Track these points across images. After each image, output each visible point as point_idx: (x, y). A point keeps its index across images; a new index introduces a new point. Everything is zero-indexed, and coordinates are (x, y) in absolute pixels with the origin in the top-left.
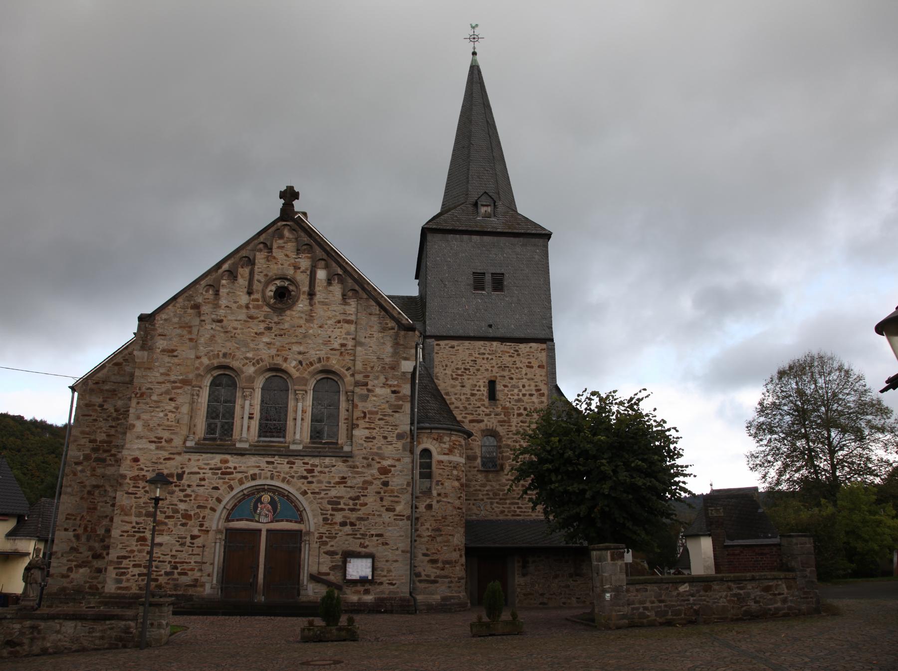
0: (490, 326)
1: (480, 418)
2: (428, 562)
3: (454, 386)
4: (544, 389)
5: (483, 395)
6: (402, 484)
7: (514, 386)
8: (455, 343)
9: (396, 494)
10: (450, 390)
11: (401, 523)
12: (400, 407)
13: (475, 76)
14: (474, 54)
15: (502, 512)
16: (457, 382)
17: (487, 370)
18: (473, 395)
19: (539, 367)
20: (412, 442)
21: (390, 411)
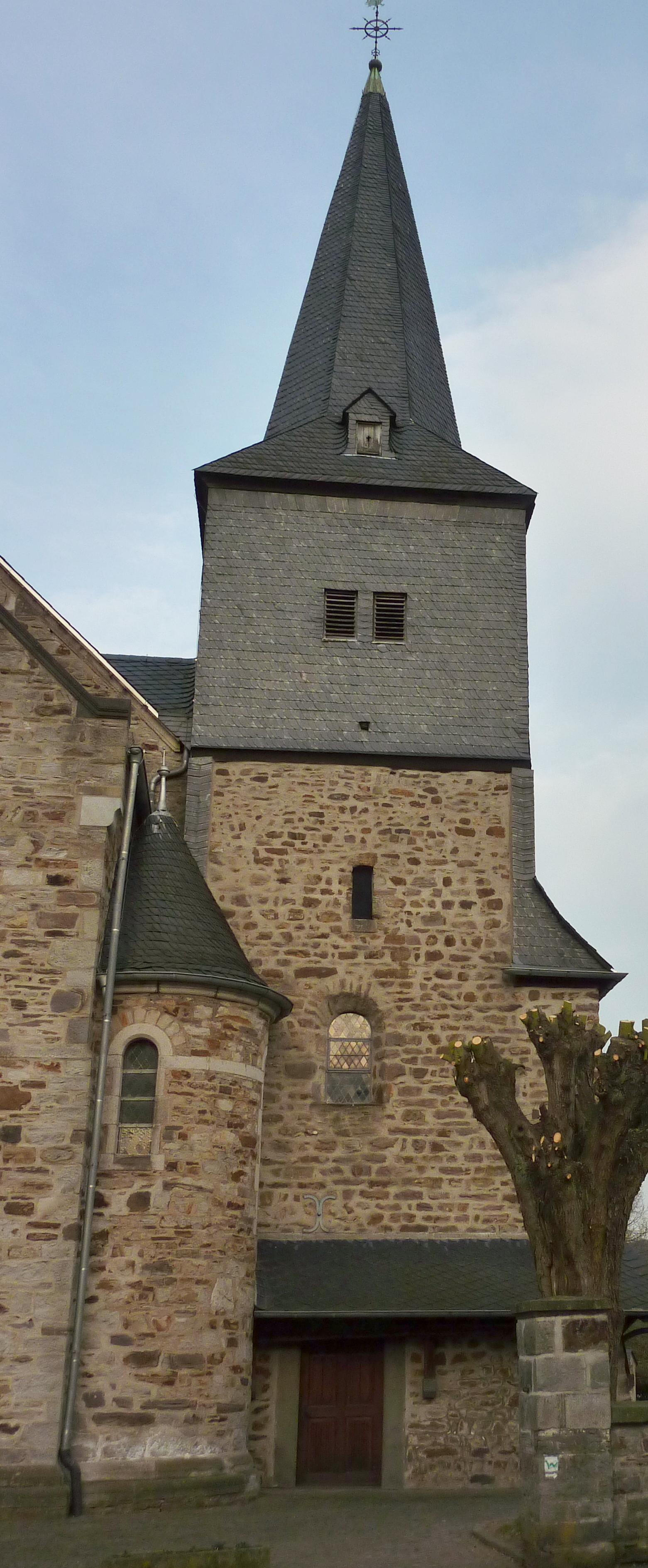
0: (364, 726)
1: (325, 963)
2: (126, 1360)
3: (258, 881)
4: (503, 892)
5: (337, 903)
6: (62, 1136)
7: (422, 882)
8: (267, 768)
9: (38, 1163)
10: (251, 890)
11: (46, 1246)
12: (70, 920)
13: (374, 121)
14: (375, 65)
15: (376, 1219)
16: (269, 871)
17: (350, 839)
18: (310, 903)
19: (490, 832)
20: (96, 1019)
21: (39, 933)
